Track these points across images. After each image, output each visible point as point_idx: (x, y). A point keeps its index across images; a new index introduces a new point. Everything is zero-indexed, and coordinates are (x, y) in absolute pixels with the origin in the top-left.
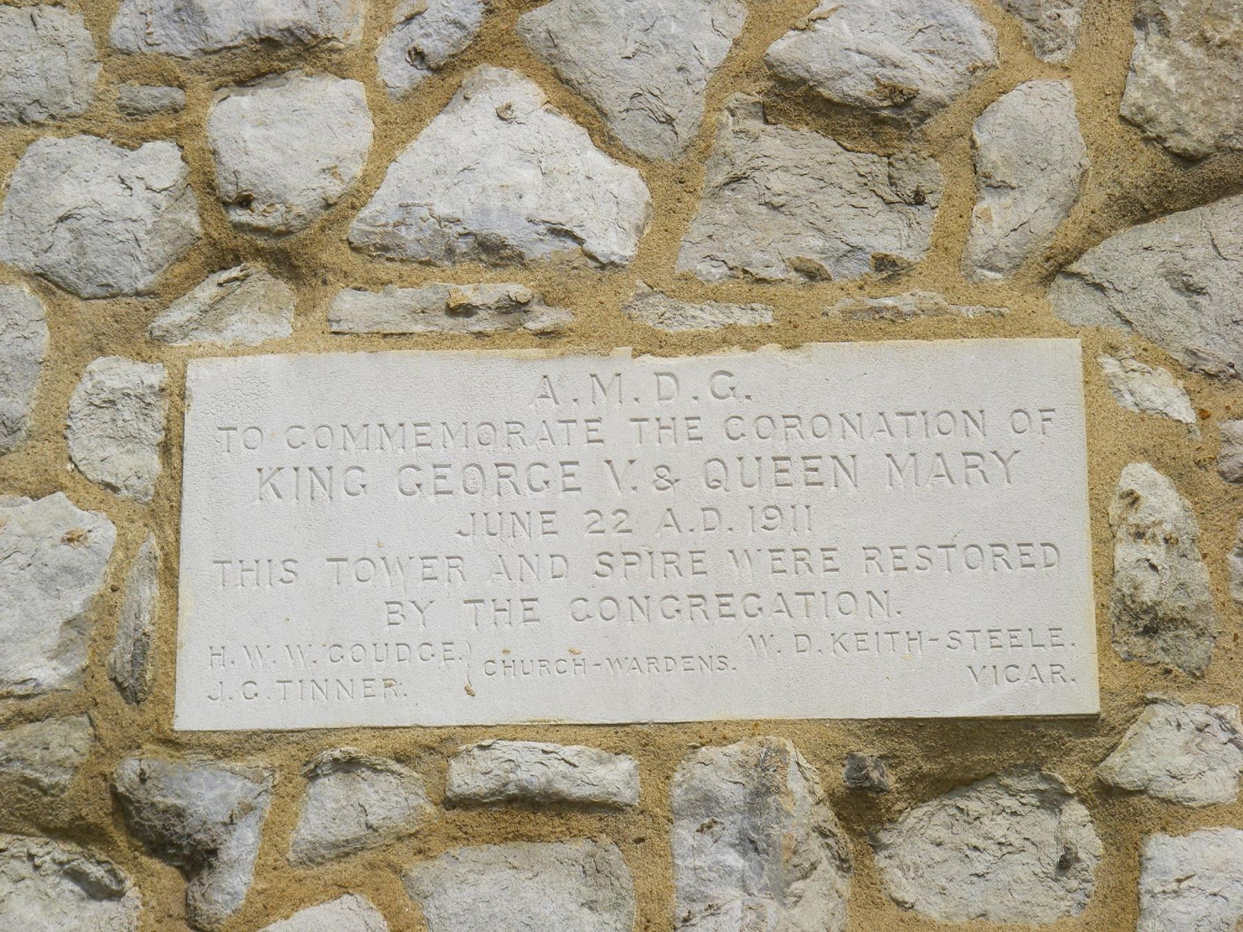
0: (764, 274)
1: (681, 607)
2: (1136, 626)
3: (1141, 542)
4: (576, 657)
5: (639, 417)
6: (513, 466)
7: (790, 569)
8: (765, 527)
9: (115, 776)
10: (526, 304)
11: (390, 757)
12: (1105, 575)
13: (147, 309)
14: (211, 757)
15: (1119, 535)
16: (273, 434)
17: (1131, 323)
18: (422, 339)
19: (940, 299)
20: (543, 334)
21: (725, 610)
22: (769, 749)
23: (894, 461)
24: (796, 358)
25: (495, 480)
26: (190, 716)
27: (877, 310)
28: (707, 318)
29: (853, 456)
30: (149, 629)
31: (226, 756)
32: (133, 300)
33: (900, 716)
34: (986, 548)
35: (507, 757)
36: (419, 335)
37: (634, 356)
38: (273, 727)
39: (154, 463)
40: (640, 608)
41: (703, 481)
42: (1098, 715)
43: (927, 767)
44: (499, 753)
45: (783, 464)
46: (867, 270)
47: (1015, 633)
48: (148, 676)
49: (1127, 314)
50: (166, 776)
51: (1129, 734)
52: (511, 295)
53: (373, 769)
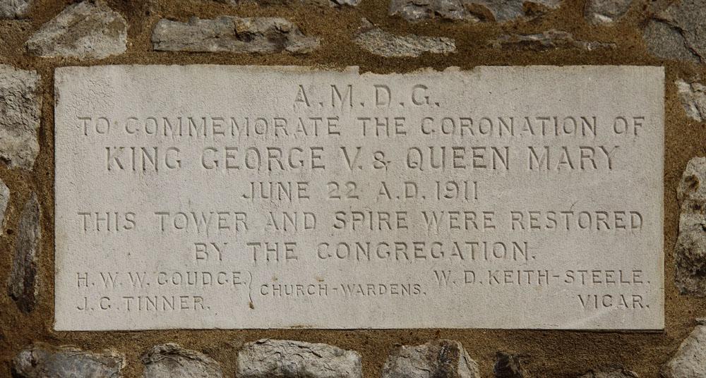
0: (448, 15)
1: (390, 251)
2: (691, 271)
3: (698, 212)
4: (320, 283)
5: (364, 116)
6: (279, 149)
7: (463, 226)
8: (446, 197)
9: (14, 362)
10: (287, 32)
11: (199, 350)
12: (672, 229)
13: (23, 29)
14: (79, 349)
15: (683, 207)
16: (116, 123)
17: (700, 57)
18: (216, 57)
19: (570, 36)
20: (296, 54)
21: (419, 253)
22: (446, 347)
23: (533, 152)
24: (470, 77)
25: (267, 159)
26: (66, 319)
27: (526, 43)
28: (408, 47)
29: (507, 148)
30: (35, 259)
31: (90, 349)
32: (14, 22)
33: (532, 328)
34: (594, 215)
35: (276, 350)
36: (215, 54)
37: (361, 73)
38: (121, 328)
39: (35, 146)
40: (363, 250)
41: (406, 163)
42: (663, 330)
43: (549, 364)
44: (270, 348)
45: (460, 152)
46: (519, 14)
47: (610, 273)
48: (36, 293)
49: (697, 50)
50: (50, 363)
51: (682, 345)
52: (278, 26)
53: (188, 357)
